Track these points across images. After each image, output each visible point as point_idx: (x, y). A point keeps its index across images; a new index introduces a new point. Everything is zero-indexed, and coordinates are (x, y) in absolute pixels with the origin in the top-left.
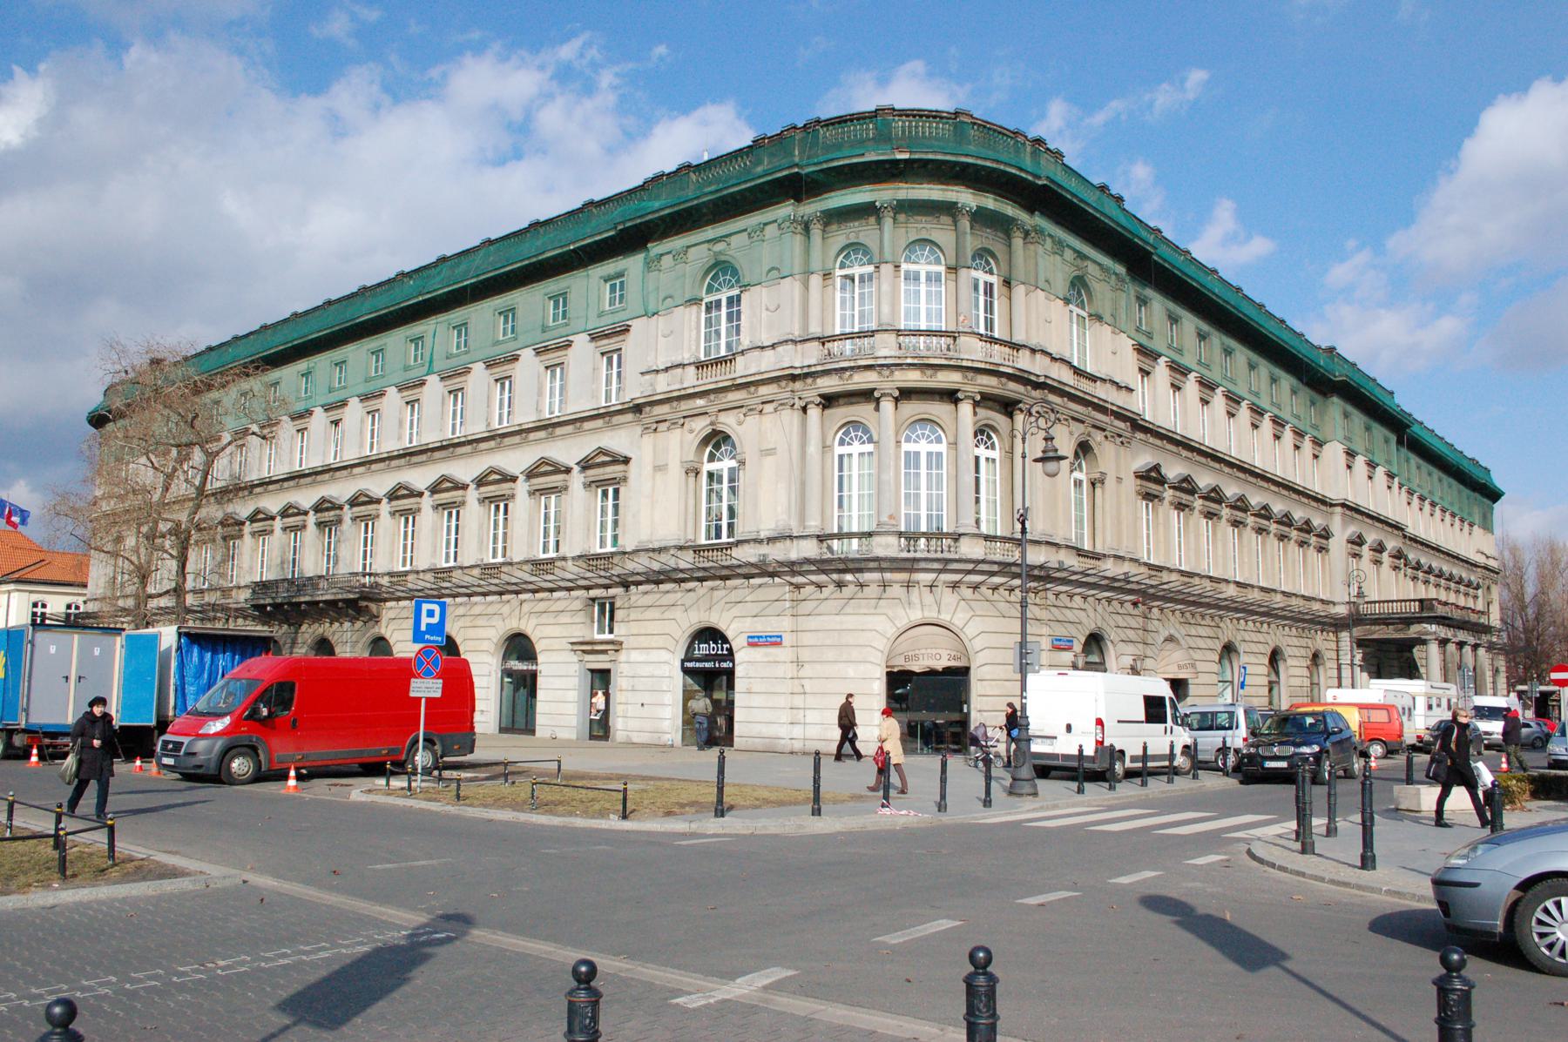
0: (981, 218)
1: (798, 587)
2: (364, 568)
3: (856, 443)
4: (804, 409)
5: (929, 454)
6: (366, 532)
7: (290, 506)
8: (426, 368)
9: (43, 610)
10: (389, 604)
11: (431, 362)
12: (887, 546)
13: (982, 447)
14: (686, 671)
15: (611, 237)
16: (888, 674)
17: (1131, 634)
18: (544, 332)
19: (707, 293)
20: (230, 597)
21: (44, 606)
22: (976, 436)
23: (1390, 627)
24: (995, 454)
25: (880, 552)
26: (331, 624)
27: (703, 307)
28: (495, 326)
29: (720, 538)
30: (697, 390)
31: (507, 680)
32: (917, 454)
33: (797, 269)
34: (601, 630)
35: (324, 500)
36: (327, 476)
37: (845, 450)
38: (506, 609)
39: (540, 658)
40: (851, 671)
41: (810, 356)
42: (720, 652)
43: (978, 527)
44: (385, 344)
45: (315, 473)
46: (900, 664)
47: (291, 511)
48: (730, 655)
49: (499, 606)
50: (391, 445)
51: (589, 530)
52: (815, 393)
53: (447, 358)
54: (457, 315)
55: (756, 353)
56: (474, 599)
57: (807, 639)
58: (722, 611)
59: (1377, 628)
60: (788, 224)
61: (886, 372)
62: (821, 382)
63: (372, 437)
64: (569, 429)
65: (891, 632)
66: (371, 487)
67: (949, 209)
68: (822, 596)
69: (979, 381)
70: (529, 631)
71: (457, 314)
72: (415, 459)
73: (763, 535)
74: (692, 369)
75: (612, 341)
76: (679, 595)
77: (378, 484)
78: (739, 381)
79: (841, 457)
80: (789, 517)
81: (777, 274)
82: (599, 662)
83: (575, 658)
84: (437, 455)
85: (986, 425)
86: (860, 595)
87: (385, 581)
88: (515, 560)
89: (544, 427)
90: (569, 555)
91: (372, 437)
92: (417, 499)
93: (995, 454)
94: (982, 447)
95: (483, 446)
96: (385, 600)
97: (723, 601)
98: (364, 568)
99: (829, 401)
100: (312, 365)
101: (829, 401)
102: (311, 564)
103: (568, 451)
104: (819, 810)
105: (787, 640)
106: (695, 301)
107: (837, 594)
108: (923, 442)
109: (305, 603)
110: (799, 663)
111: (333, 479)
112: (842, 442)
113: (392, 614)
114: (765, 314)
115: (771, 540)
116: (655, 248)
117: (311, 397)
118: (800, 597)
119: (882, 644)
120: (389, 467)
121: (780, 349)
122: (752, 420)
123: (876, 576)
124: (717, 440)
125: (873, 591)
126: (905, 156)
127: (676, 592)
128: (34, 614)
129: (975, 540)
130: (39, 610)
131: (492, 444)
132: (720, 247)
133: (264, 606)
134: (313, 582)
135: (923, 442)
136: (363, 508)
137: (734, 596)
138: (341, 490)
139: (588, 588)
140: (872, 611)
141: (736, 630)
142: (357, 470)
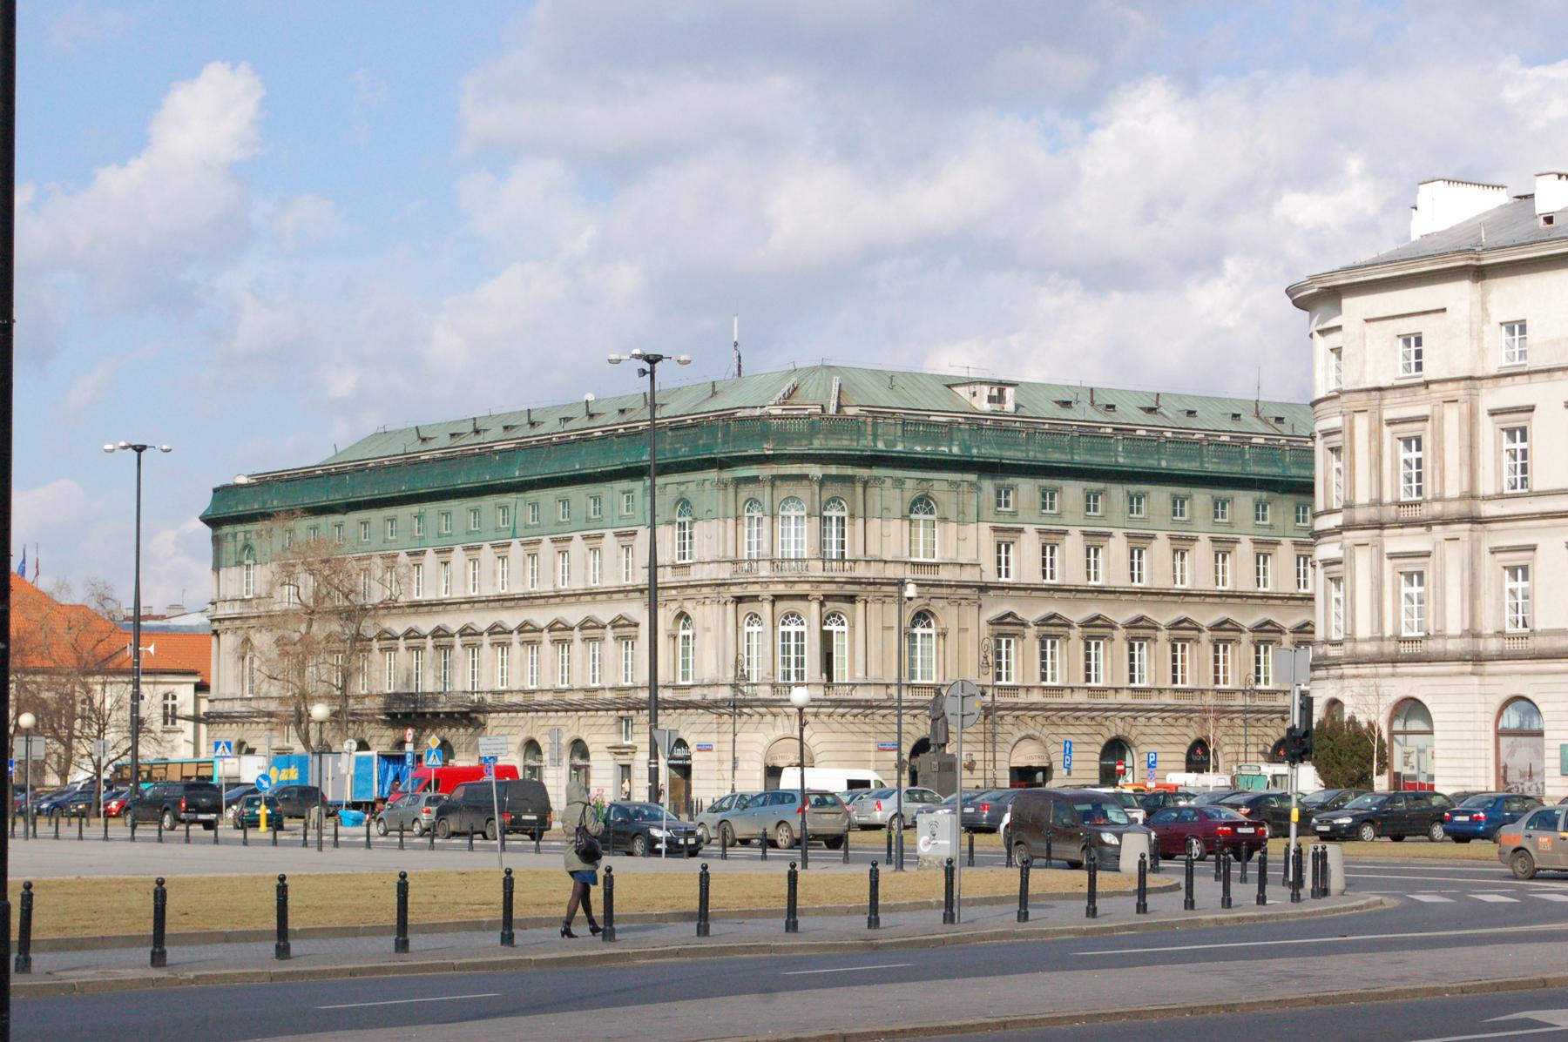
0: (825, 480)
1: (721, 715)
2: (473, 688)
3: (756, 625)
4: (725, 603)
5: (797, 633)
6: (473, 657)
7: (412, 630)
9: (174, 702)
10: (492, 715)
11: (514, 528)
12: (765, 692)
14: (671, 766)
17: (1086, 739)
18: (587, 522)
20: (363, 704)
21: (174, 698)
24: (845, 629)
25: (761, 696)
26: (450, 729)
27: (677, 525)
28: (557, 511)
29: (688, 680)
31: (574, 772)
32: (789, 633)
33: (721, 515)
34: (627, 739)
35: (439, 629)
36: (441, 608)
37: (785, 629)
38: (570, 722)
39: (592, 757)
41: (725, 572)
45: (430, 604)
47: (412, 634)
48: (689, 758)
49: (565, 720)
50: (488, 591)
51: (617, 670)
53: (526, 528)
54: (531, 495)
55: (700, 566)
56: (550, 714)
61: (765, 586)
63: (474, 580)
64: (604, 597)
65: (766, 742)
66: (476, 622)
67: (804, 477)
70: (584, 738)
73: (706, 682)
74: (669, 569)
77: (482, 621)
78: (692, 583)
79: (748, 633)
80: (718, 672)
81: (710, 515)
82: (624, 760)
83: (610, 757)
84: (522, 603)
87: (489, 699)
88: (575, 687)
89: (590, 594)
90: (607, 686)
91: (474, 580)
93: (845, 629)
95: (552, 600)
96: (490, 712)
98: (473, 688)
99: (739, 600)
100: (423, 510)
101: (739, 600)
102: (429, 685)
103: (541, 617)
105: (715, 748)
108: (793, 625)
109: (429, 713)
111: (445, 611)
113: (495, 723)
114: (705, 539)
115: (709, 686)
117: (423, 538)
119: (761, 750)
120: (488, 608)
121: (712, 565)
122: (700, 608)
125: (756, 718)
128: (166, 707)
129: (818, 687)
131: (558, 600)
132: (683, 488)
133: (396, 714)
134: (434, 697)
135: (793, 625)
136: (470, 638)
137: (691, 719)
138: (453, 622)
139: (618, 710)
141: (691, 740)
142: (464, 606)
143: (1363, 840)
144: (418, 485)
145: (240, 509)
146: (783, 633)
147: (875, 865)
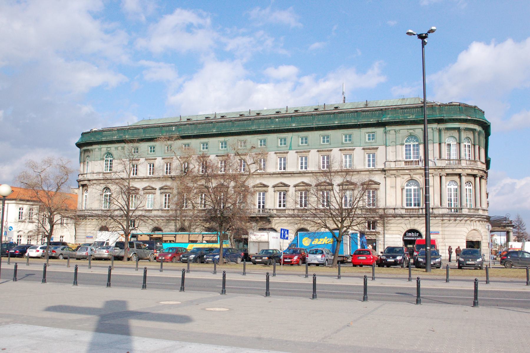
1: (443, 220)
8: (289, 147)
10: (275, 218)
12: (466, 211)
13: (467, 186)
15: (375, 123)
16: (467, 241)
19: (406, 142)
22: (466, 183)
23: (500, 228)
24: (471, 188)
26: (206, 223)
30: (407, 168)
37: (449, 187)
40: (458, 240)
42: (415, 235)
43: (467, 207)
44: (267, 138)
46: (471, 239)
52: (445, 173)
53: (298, 146)
57: (446, 233)
58: (419, 225)
59: (496, 228)
60: (436, 129)
61: (464, 170)
62: (446, 170)
68: (450, 223)
69: (390, 172)
71: (302, 134)
72: (284, 175)
74: (102, 174)
75: (371, 151)
76: (403, 221)
85: (470, 181)
86: (460, 223)
92: (288, 188)
93: (471, 188)
94: (467, 186)
96: (273, 217)
97: (419, 223)
104: (184, 288)
105: (440, 233)
106: (402, 144)
107: (454, 222)
110: (444, 238)
112: (448, 185)
113: (277, 221)
116: (388, 128)
118: (443, 223)
119: (466, 234)
123: (453, 218)
124: (107, 189)
125: (463, 222)
126: (470, 118)
127: (402, 220)
130: (21, 211)
132: (108, 149)
140: (463, 227)
143: (482, 269)
144: (445, 115)
145: (126, 137)
146: (448, 188)
147: (16, 264)
